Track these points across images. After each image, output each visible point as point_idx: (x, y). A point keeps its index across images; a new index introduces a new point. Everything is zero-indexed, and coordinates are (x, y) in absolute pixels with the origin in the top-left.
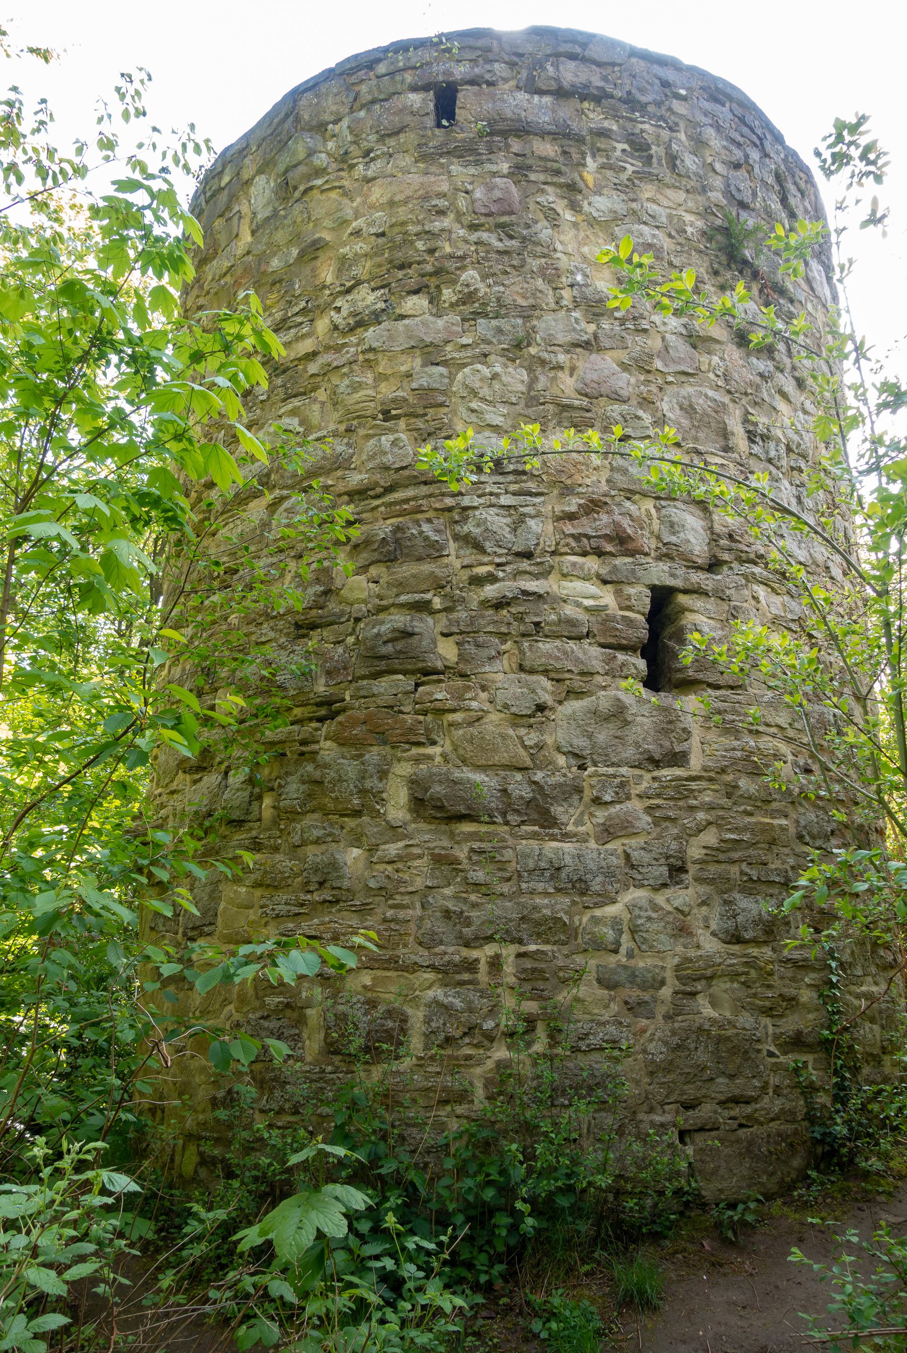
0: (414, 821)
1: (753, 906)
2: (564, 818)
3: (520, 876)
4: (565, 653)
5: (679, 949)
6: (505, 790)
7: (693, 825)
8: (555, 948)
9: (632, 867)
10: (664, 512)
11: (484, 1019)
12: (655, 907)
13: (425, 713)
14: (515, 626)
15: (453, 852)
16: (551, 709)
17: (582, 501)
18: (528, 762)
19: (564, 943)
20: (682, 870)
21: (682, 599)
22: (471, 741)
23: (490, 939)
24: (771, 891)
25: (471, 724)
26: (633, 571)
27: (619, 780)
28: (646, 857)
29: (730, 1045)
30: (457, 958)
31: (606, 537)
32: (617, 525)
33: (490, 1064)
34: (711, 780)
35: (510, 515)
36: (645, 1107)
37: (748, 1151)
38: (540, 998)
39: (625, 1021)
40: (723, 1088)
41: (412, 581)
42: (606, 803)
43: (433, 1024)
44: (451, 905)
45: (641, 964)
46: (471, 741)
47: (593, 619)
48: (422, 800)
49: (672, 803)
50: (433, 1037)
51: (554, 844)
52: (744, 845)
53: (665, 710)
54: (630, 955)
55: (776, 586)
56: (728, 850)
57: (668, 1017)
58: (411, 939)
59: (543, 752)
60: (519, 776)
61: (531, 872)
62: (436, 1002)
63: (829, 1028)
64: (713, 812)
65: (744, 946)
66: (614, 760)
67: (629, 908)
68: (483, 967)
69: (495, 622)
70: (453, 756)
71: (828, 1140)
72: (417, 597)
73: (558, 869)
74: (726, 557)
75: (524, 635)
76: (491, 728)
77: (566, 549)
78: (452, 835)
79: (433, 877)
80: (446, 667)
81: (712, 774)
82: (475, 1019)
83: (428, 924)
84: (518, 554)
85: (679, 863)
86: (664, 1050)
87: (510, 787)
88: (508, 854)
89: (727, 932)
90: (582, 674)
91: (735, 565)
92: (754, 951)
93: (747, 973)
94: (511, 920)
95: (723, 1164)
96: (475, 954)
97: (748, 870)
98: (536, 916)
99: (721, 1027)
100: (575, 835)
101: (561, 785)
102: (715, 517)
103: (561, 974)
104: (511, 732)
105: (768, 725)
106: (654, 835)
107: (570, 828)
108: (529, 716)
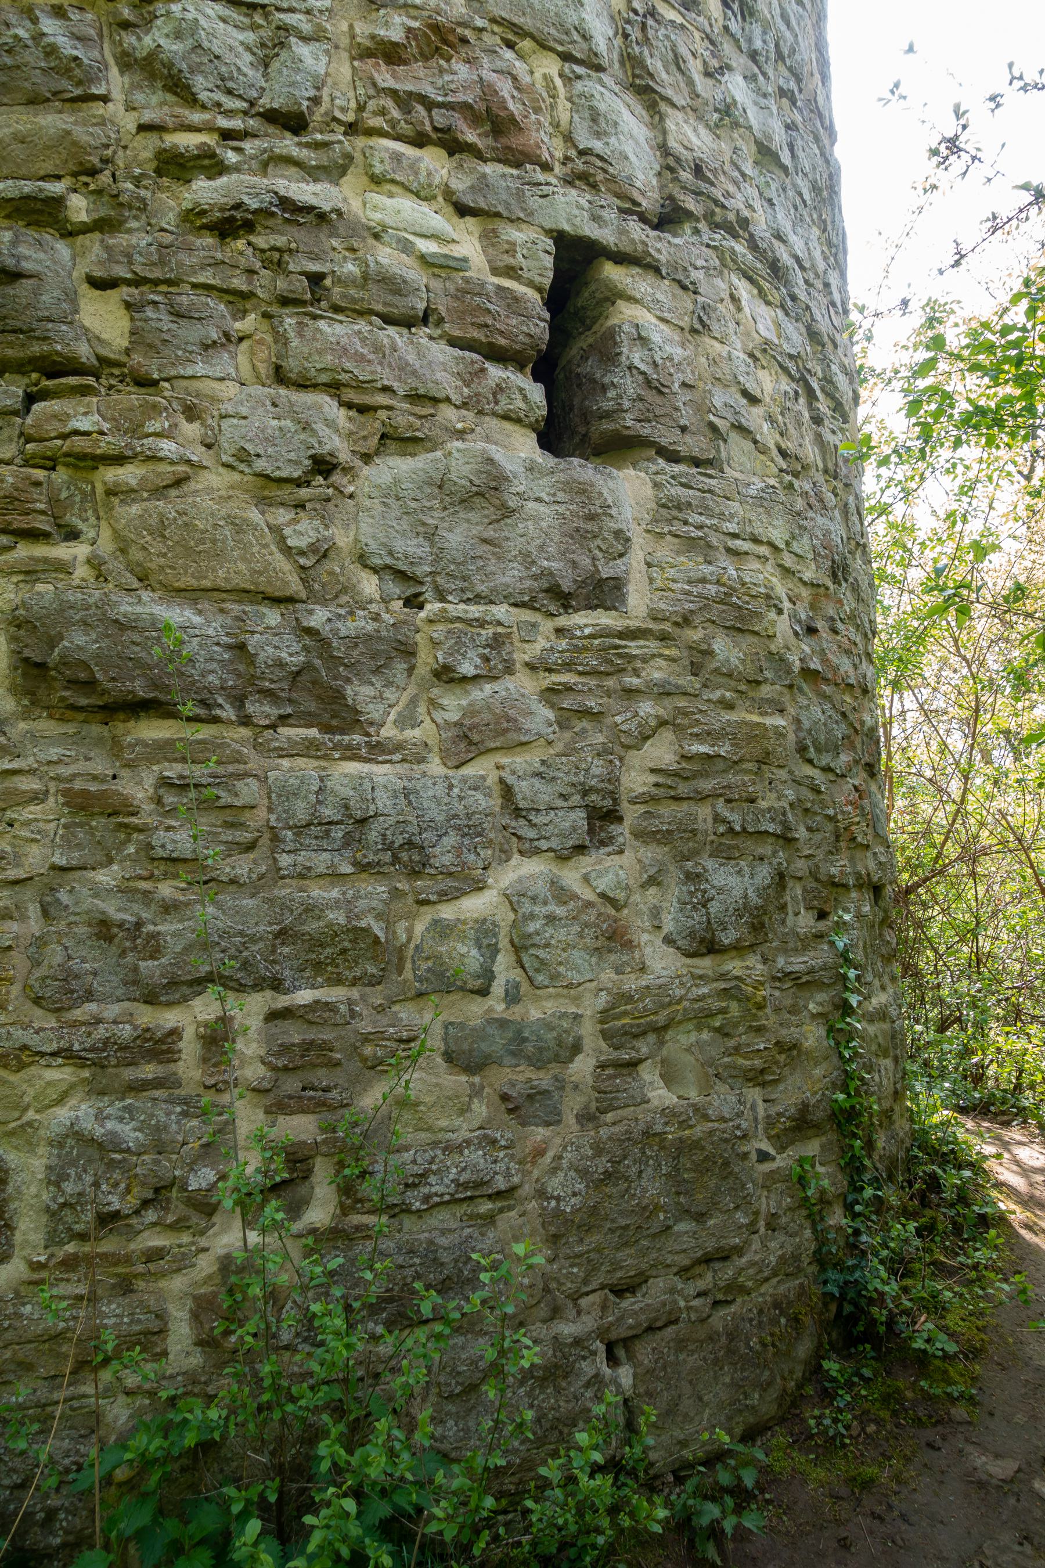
0: (25, 715)
1: (733, 881)
2: (373, 711)
3: (275, 839)
4: (378, 349)
5: (608, 976)
6: (242, 647)
7: (632, 726)
8: (355, 993)
9: (517, 812)
10: (579, 86)
11: (192, 1167)
12: (562, 894)
13: (50, 463)
14: (265, 284)
15: (118, 786)
16: (347, 470)
17: (416, 24)
18: (295, 586)
19: (374, 981)
20: (613, 816)
21: (612, 272)
22: (160, 531)
23: (200, 984)
24: (760, 851)
25: (159, 491)
26: (520, 195)
27: (490, 631)
28: (545, 793)
29: (698, 1157)
30: (126, 1032)
31: (465, 108)
32: (488, 91)
33: (206, 1265)
34: (664, 637)
35: (254, 27)
36: (543, 1311)
37: (730, 1352)
38: (321, 1106)
39: (503, 1136)
40: (688, 1242)
41: (18, 151)
42: (464, 679)
43: (69, 1187)
44: (113, 909)
45: (535, 1014)
46: (160, 531)
47: (436, 285)
48: (42, 666)
49: (593, 682)
50: (68, 1216)
51: (353, 767)
52: (721, 765)
53: (582, 491)
54: (512, 997)
55: (766, 286)
56: (695, 775)
57: (586, 1118)
58: (15, 990)
59: (327, 565)
60: (273, 617)
61: (300, 829)
62: (75, 1134)
63: (845, 1089)
64: (667, 702)
65: (718, 958)
66: (481, 588)
67: (512, 899)
68: (189, 1047)
69: (219, 263)
70: (115, 565)
71: (851, 1294)
72: (28, 187)
73: (363, 821)
74: (690, 203)
75: (285, 301)
76: (207, 503)
77: (377, 122)
78: (116, 748)
79: (68, 844)
80: (103, 361)
81: (667, 626)
82: (169, 1167)
83: (55, 954)
84: (272, 117)
85: (608, 803)
86: (580, 1187)
87: (253, 642)
88: (249, 791)
89: (692, 935)
90: (415, 397)
91: (702, 226)
92: (734, 966)
93: (723, 1011)
94: (254, 939)
95: (686, 1389)
96: (170, 1018)
97: (726, 813)
98: (312, 926)
99: (684, 1124)
100: (399, 747)
101: (368, 638)
102: (670, 125)
103: (368, 1050)
104: (254, 515)
105: (756, 540)
106: (559, 747)
107: (388, 732)
108: (298, 483)
